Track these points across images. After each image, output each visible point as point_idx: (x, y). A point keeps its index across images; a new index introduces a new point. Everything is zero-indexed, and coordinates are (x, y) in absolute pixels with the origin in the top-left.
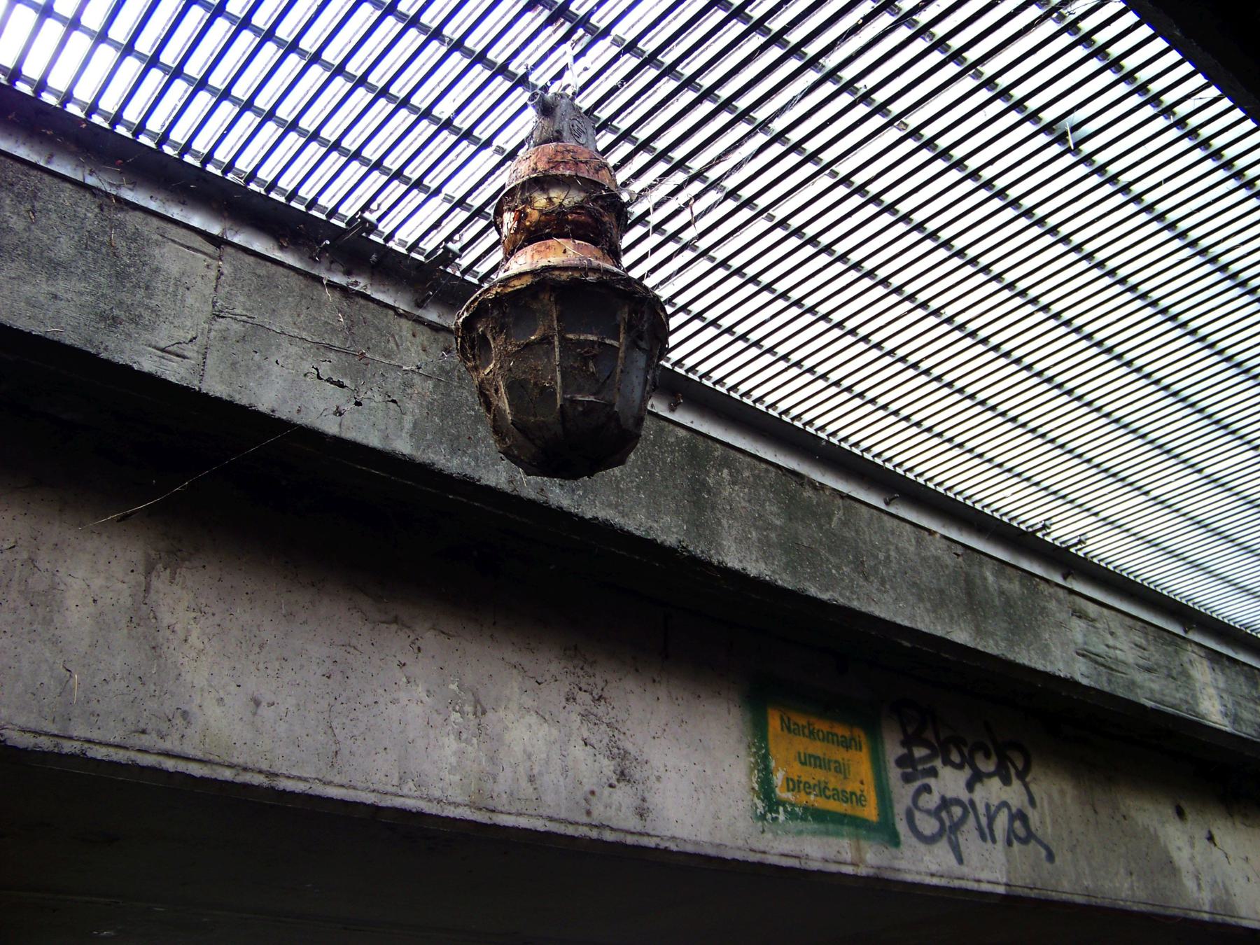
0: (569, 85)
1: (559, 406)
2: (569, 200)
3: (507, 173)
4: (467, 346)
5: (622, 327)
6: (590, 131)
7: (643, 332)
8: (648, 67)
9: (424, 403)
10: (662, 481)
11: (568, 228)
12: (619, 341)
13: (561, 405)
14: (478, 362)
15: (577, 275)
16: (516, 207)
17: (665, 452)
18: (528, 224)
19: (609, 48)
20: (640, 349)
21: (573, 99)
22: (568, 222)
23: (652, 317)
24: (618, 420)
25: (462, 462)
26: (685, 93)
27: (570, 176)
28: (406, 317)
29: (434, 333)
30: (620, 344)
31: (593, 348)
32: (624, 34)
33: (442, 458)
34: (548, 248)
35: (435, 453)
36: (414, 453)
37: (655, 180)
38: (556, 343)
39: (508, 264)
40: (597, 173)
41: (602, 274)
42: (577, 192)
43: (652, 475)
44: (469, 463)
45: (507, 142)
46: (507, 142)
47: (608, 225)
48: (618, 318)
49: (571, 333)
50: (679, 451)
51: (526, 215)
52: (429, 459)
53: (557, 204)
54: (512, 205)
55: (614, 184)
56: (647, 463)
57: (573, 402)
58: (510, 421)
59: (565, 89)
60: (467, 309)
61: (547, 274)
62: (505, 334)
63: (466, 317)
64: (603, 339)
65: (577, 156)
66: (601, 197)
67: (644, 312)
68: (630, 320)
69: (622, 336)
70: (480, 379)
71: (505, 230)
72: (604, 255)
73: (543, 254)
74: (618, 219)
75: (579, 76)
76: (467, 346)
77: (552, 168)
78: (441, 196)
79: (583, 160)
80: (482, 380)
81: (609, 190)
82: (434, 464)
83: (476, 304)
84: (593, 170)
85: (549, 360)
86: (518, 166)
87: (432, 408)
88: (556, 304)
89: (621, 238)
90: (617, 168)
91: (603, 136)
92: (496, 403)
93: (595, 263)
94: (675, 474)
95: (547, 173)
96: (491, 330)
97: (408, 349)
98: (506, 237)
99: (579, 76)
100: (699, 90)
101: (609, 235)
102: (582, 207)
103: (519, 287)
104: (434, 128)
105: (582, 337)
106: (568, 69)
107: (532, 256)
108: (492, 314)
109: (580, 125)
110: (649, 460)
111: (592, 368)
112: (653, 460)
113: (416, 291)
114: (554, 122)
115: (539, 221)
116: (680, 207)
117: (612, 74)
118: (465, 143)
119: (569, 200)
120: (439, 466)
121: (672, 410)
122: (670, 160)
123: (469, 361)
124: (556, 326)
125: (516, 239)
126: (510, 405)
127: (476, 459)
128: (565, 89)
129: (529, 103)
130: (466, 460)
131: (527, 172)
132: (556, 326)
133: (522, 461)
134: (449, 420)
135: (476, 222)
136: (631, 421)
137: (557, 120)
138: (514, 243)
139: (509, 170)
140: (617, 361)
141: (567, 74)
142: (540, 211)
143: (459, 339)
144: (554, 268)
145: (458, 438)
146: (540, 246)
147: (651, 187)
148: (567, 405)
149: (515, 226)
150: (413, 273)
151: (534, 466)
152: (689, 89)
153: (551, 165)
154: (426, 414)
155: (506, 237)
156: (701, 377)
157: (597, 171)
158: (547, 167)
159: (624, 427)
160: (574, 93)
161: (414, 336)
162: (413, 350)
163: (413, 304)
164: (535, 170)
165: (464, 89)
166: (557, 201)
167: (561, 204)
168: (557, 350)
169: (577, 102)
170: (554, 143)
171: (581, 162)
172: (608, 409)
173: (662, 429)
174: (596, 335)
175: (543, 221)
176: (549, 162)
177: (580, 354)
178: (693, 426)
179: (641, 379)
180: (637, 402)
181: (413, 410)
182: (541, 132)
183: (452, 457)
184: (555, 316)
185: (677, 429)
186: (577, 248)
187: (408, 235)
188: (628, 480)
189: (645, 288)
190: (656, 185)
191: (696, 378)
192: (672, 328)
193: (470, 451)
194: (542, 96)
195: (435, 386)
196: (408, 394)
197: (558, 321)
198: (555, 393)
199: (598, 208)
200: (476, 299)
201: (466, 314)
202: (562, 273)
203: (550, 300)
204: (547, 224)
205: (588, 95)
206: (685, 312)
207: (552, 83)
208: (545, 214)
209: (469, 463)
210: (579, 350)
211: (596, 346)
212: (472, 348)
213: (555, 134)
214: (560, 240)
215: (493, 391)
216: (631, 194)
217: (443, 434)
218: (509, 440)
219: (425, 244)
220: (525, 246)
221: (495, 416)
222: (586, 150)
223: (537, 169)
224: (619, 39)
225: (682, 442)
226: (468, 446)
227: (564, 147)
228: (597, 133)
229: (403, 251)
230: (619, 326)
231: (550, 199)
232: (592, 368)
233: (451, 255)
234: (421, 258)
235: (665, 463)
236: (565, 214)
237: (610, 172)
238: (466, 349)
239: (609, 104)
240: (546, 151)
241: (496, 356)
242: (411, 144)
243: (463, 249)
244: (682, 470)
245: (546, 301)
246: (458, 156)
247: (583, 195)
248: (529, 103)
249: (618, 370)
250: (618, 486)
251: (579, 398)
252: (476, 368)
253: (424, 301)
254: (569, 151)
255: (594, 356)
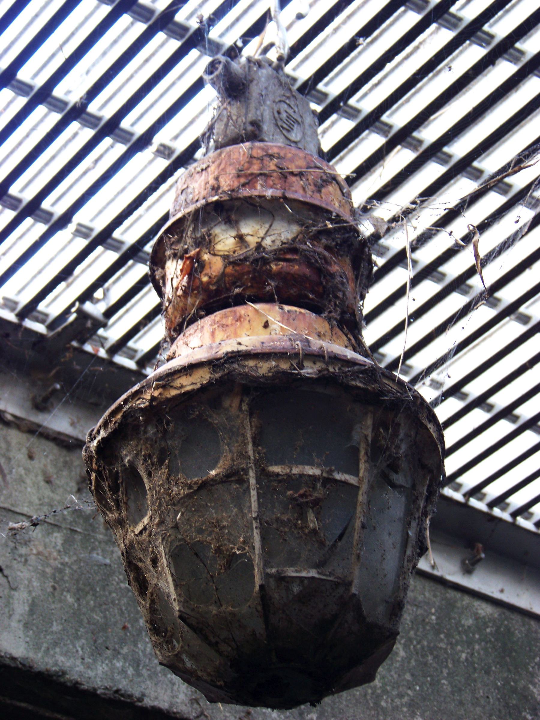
0: (272, 45)
1: (257, 588)
2: (273, 238)
3: (172, 194)
4: (105, 485)
5: (362, 453)
6: (309, 119)
7: (398, 458)
8: (402, 9)
9: (48, 570)
10: (453, 693)
11: (271, 286)
12: (357, 475)
13: (261, 587)
14: (124, 514)
15: (284, 366)
16: (186, 251)
17: (457, 643)
18: (205, 279)
19: (151, 162)
20: (394, 486)
21: (278, 68)
22: (271, 275)
23: (413, 433)
24: (358, 607)
25: (113, 669)
26: (466, 48)
27: (274, 199)
28: (18, 427)
29: (64, 452)
30: (360, 481)
31: (314, 488)
32: (92, 220)
33: (78, 662)
34: (239, 319)
35: (66, 654)
36: (31, 655)
37: (414, 203)
38: (252, 481)
39: (174, 347)
40: (319, 191)
41: (327, 364)
42: (285, 225)
43: (435, 683)
44: (123, 671)
45: (176, 137)
46: (176, 137)
47: (339, 279)
48: (356, 437)
49: (276, 464)
50: (480, 641)
51: (202, 265)
52: (56, 664)
53: (253, 245)
54: (179, 247)
55: (348, 208)
56: (425, 664)
57: (281, 579)
58: (177, 614)
59: (266, 50)
60: (105, 425)
61: (236, 366)
62: (168, 467)
63: (103, 439)
64: (330, 472)
65: (285, 164)
66: (327, 232)
67: (398, 425)
68: (375, 439)
69: (362, 466)
70: (127, 542)
71: (168, 291)
72: (332, 329)
73: (230, 330)
74: (356, 266)
75: (288, 28)
76: (105, 485)
77: (244, 185)
78: (72, 227)
79: (296, 170)
80: (132, 545)
81: (338, 219)
82: (64, 673)
83: (119, 416)
84: (312, 187)
85: (241, 509)
86: (188, 182)
87: (62, 579)
88: (251, 414)
89: (363, 297)
90: (351, 181)
91: (333, 123)
92: (154, 581)
93: (316, 343)
94: (475, 681)
95: (235, 195)
96: (145, 460)
97: (21, 480)
98: (170, 301)
99: (288, 28)
100: (488, 43)
101: (340, 294)
102: (294, 250)
103: (189, 388)
104: (56, 117)
105: (296, 471)
106: (271, 19)
107: (213, 334)
108: (145, 432)
109: (290, 111)
110: (430, 658)
111: (312, 521)
112: (436, 657)
113: (33, 384)
114: (247, 108)
115: (223, 274)
116: (457, 244)
117: (344, 22)
118: (107, 141)
119: (273, 238)
120: (73, 676)
121: (468, 571)
122: (445, 159)
123: (110, 510)
124: (251, 453)
125: (185, 304)
126: (176, 586)
127: (136, 663)
128: (266, 50)
129: (207, 78)
130: (119, 664)
131: (203, 193)
132: (251, 453)
133: (199, 678)
134: (89, 597)
135: (130, 268)
136: (381, 609)
137: (253, 105)
138: (184, 310)
139: (174, 189)
140: (355, 508)
141: (270, 27)
142: (225, 257)
143: (94, 475)
144: (248, 355)
145: (104, 628)
146: (226, 316)
147: (407, 213)
148: (272, 583)
149: (184, 282)
150: (29, 354)
151: (220, 687)
152: (473, 42)
153: (243, 180)
154: (50, 590)
155: (170, 301)
156: (514, 515)
157: (319, 188)
158: (236, 184)
159: (369, 620)
160: (280, 59)
161: (31, 457)
162: (28, 481)
163: (28, 404)
164: (215, 189)
165: (104, 54)
166: (252, 241)
167: (259, 246)
168: (253, 493)
169: (288, 69)
170: (248, 144)
171: (292, 174)
172: (341, 590)
173: (451, 605)
174: (318, 466)
175: (232, 275)
176: (239, 176)
177: (292, 499)
178: (505, 597)
179: (398, 538)
180: (391, 576)
181: (30, 581)
182: (227, 125)
183: (95, 661)
184: (249, 436)
185: (477, 603)
186: (287, 318)
187: (20, 292)
188: (395, 693)
189: (401, 383)
190: (414, 210)
191: (506, 516)
192: (449, 443)
193: (125, 650)
194: (227, 67)
195: (68, 542)
196: (21, 556)
197: (256, 444)
198: (250, 566)
199: (320, 250)
200: (120, 407)
201: (103, 434)
202: (261, 364)
203: (240, 408)
204: (236, 281)
205: (306, 58)
206: (483, 409)
207: (245, 43)
208: (234, 263)
209: (123, 671)
210: (289, 493)
211: (319, 485)
212: (115, 489)
213: (250, 128)
214: (258, 306)
215: (148, 562)
216: (376, 223)
217: (80, 622)
218: (178, 643)
219: (48, 306)
220: (201, 317)
221: (153, 602)
222: (301, 154)
223: (219, 187)
224: (84, 230)
225: (486, 625)
226: (122, 642)
227: (263, 149)
228: (320, 124)
229: (11, 317)
230: (357, 450)
231: (240, 238)
232: (312, 521)
233: (89, 324)
234: (40, 328)
235: (457, 662)
236: (266, 261)
237: (341, 189)
238: (104, 492)
239: (341, 71)
240: (235, 156)
241: (153, 504)
242: (20, 144)
243: (110, 312)
244: (487, 673)
245: (234, 411)
246: (96, 161)
247: (295, 229)
248: (207, 78)
249: (358, 524)
250: (377, 704)
251: (291, 572)
252: (121, 523)
253: (46, 400)
254: (271, 156)
255: (316, 503)
